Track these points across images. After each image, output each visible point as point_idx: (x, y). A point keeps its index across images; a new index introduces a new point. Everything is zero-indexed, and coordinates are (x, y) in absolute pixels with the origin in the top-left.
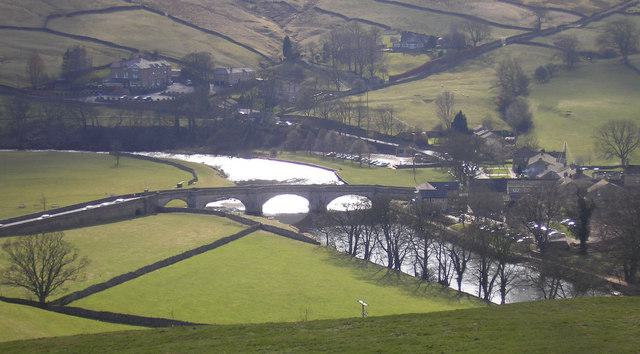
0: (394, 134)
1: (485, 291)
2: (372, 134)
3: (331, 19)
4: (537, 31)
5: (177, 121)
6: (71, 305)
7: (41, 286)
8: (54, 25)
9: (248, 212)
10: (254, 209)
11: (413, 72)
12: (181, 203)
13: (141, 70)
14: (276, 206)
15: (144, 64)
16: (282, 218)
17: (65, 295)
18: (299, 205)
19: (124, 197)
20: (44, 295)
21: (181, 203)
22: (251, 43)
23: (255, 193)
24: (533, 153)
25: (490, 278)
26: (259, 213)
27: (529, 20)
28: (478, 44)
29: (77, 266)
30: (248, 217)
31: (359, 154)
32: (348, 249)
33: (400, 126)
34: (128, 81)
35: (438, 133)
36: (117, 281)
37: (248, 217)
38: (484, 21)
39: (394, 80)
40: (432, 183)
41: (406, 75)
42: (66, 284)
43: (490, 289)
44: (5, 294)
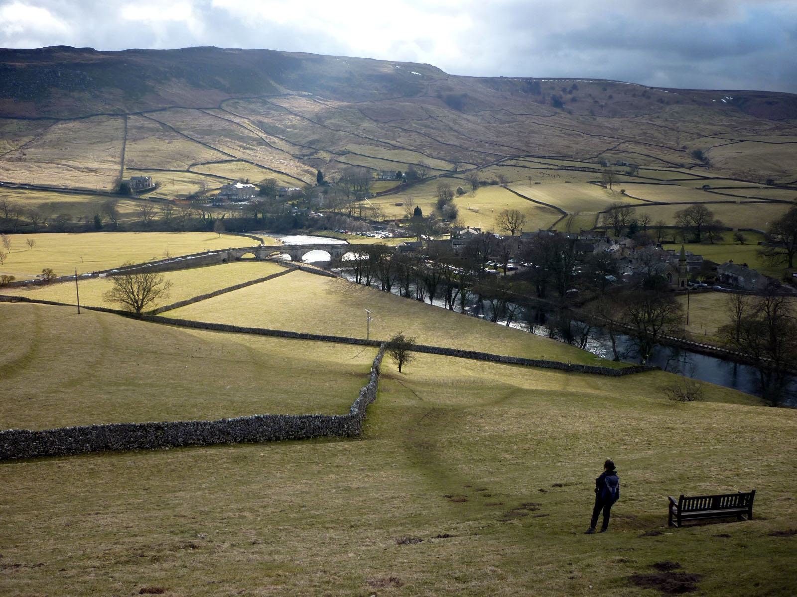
0: (380, 220)
1: (450, 304)
2: (368, 221)
3: (344, 166)
4: (455, 172)
5: (256, 215)
6: (159, 315)
7: (137, 302)
8: (191, 169)
9: (293, 260)
10: (297, 258)
11: (390, 190)
12: (251, 255)
13: (237, 189)
14: (310, 257)
15: (239, 186)
16: (316, 264)
17: (156, 308)
18: (325, 256)
19: (212, 252)
20: (139, 308)
21: (251, 255)
22: (300, 177)
23: (297, 252)
24: (463, 229)
25: (453, 295)
26: (300, 260)
27: (450, 167)
28: (424, 177)
29: (162, 288)
30: (293, 263)
31: (276, 196)
32: (355, 280)
33: (384, 216)
34: (230, 195)
35: (405, 220)
36: (196, 300)
37: (293, 263)
38: (428, 168)
39: (379, 194)
40: (405, 243)
41: (385, 192)
42: (156, 300)
43: (453, 303)
44: (6, 177)
